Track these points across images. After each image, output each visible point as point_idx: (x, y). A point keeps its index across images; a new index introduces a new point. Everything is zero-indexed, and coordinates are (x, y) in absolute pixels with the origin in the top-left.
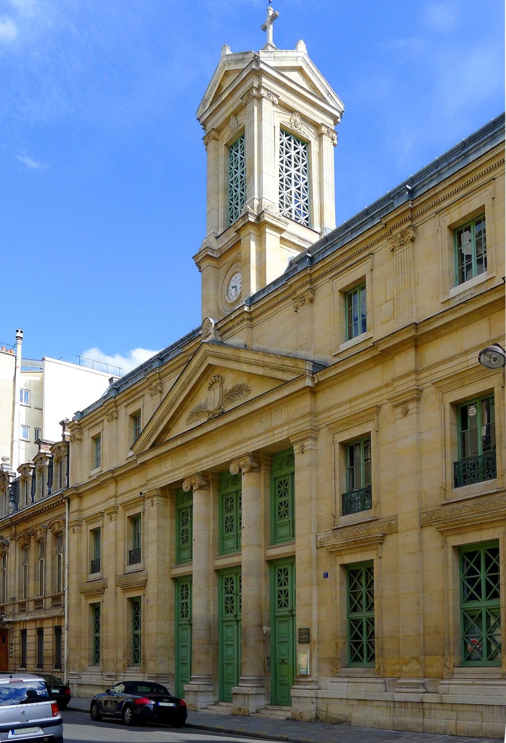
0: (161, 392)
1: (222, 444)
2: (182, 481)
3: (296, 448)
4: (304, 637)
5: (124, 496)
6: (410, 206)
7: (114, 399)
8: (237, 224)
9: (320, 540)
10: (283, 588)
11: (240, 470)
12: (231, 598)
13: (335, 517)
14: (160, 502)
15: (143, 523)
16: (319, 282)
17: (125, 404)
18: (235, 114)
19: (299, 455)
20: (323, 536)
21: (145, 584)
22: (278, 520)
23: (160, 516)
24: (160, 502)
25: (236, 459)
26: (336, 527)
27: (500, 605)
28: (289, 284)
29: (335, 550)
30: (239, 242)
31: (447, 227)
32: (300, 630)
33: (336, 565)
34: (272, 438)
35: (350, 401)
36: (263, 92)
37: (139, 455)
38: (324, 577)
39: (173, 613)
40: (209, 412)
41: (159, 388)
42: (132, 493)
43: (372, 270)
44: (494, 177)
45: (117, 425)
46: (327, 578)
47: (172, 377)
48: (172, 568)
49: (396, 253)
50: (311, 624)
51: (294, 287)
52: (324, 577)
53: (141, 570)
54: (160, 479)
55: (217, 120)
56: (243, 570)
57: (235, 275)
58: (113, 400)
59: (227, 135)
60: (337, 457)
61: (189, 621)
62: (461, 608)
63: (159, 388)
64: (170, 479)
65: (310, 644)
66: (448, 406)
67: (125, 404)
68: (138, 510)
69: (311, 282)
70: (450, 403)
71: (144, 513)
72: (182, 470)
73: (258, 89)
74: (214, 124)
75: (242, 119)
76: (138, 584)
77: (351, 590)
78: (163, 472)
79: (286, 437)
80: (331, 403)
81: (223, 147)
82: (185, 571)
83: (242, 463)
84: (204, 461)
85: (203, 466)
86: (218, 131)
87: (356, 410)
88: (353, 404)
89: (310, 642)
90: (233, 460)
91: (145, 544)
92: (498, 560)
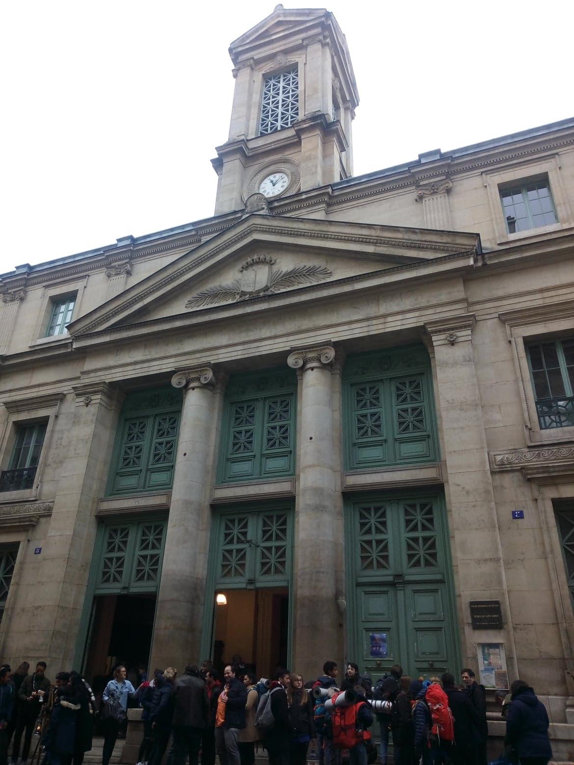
0: (129, 273)
1: (265, 332)
2: (170, 374)
3: (438, 340)
4: (489, 616)
5: (41, 388)
6: (132, 248)
7: (28, 275)
8: (301, 124)
9: (502, 460)
10: (374, 537)
11: (188, 383)
12: (238, 551)
13: (530, 429)
14: (102, 403)
15: (53, 431)
16: (459, 176)
17: (44, 284)
18: (286, 52)
19: (443, 349)
20: (507, 456)
21: (37, 523)
22: (232, 454)
23: (99, 421)
24: (102, 403)
25: (302, 349)
26: (533, 444)
27: (4, 607)
28: (4, 282)
29: (546, 475)
30: (299, 143)
31: (48, 298)
32: (471, 603)
33: (543, 499)
34: (380, 327)
35: (542, 291)
36: (328, 40)
37: (77, 338)
38: (514, 518)
39: (87, 574)
40: (243, 293)
41: (128, 267)
42: (36, 389)
43: (85, 287)
44: (89, 274)
45: (19, 307)
46: (520, 521)
47: (151, 259)
48: (102, 500)
49: (112, 278)
50: (503, 594)
51: (111, 259)
52: (514, 518)
53: (33, 499)
54: (113, 371)
55: (269, 50)
56: (301, 502)
57: (271, 177)
58: (132, 248)
59: (268, 67)
60: (7, 436)
61: (124, 588)
62: (569, 587)
63: (128, 267)
64: (134, 372)
65: (502, 631)
66: (11, 424)
67: (44, 284)
68: (41, 413)
69: (131, 258)
70: (13, 422)
71: (57, 417)
72: (173, 360)
73: (325, 37)
74: (255, 55)
75: (294, 58)
76: (20, 522)
77: (4, 575)
78: (431, 303)
79: (422, 324)
80: (500, 293)
81: (261, 76)
82: (137, 504)
83: (310, 355)
84: (223, 351)
85: (221, 356)
86: (258, 62)
87: (548, 301)
88: (546, 294)
89: (505, 626)
90: (294, 350)
91: (50, 461)
92: (15, 563)
